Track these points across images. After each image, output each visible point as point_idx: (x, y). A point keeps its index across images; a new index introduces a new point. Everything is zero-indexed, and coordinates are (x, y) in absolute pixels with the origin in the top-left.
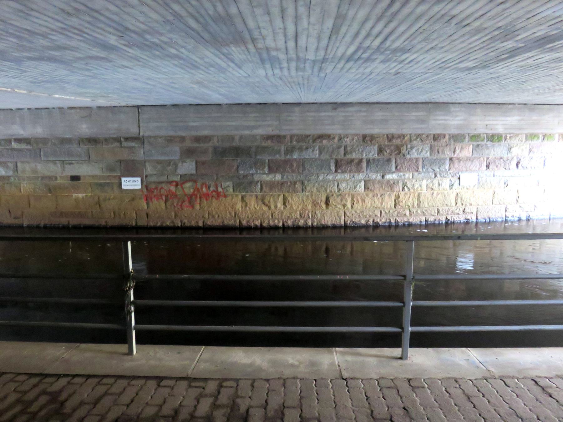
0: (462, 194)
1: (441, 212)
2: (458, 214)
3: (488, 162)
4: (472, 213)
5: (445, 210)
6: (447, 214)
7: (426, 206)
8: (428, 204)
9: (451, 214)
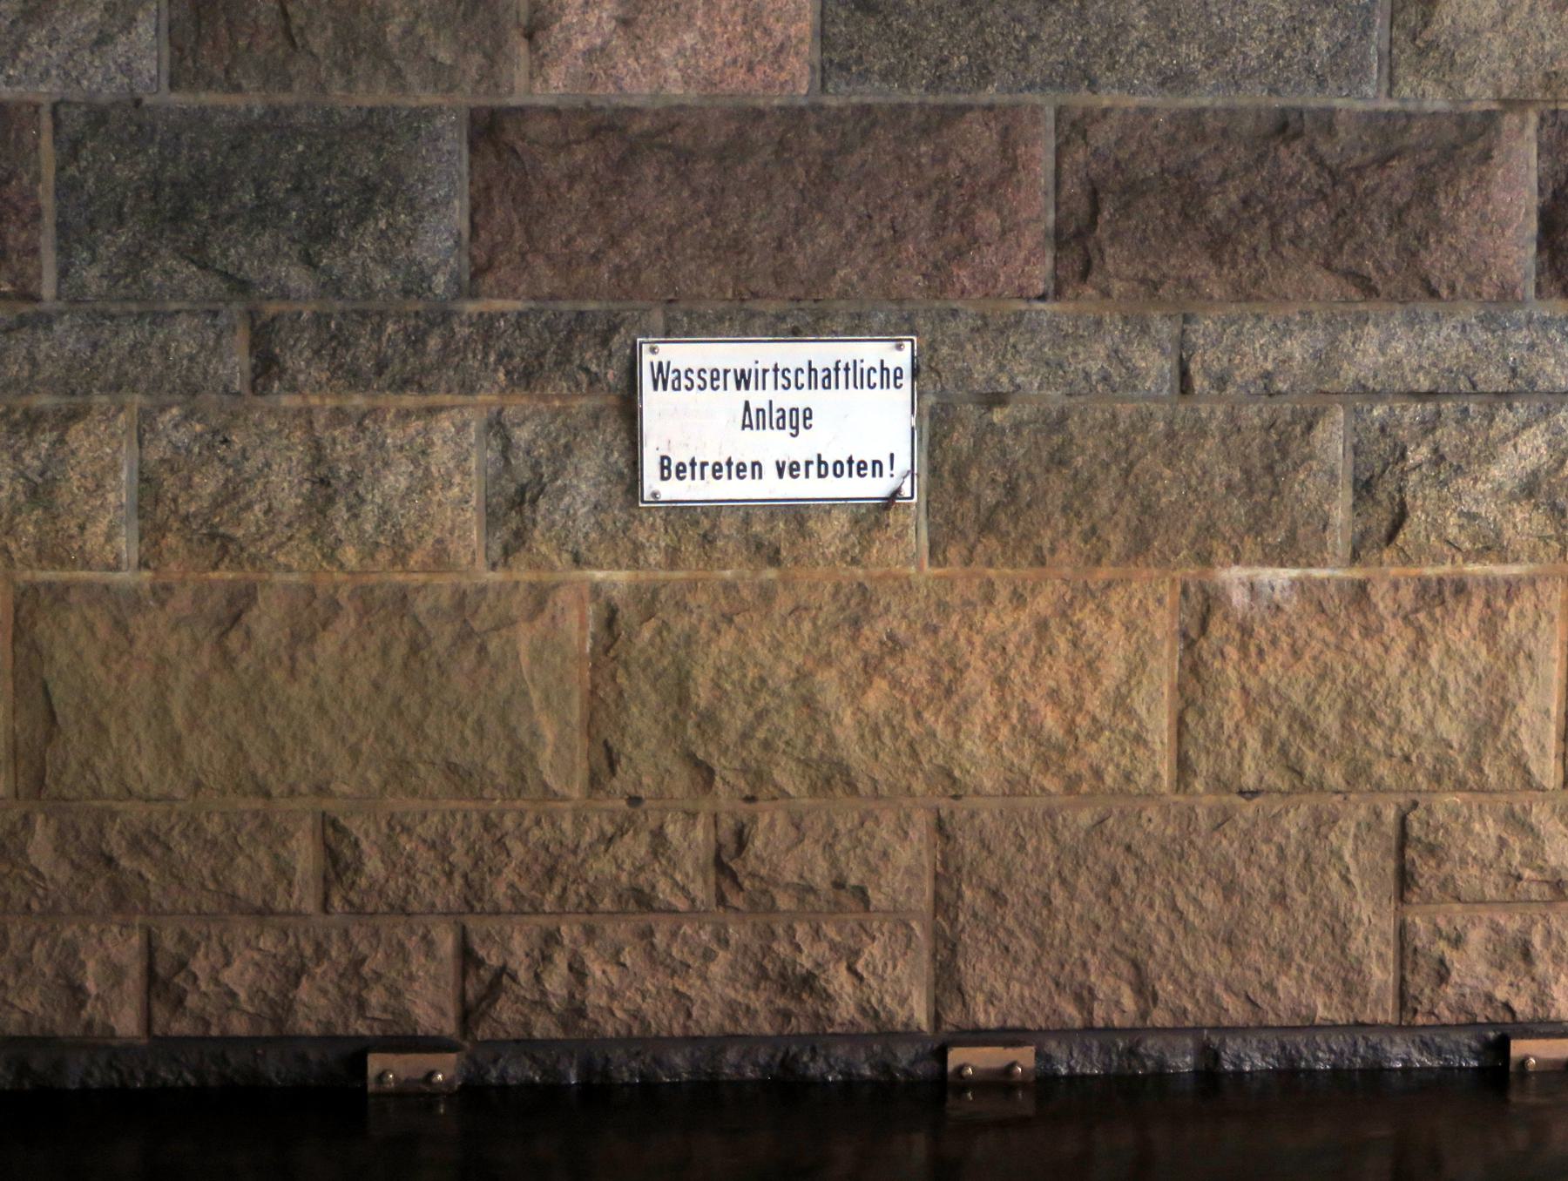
0: (681, 624)
1: (374, 865)
2: (643, 900)
3: (1072, 187)
4: (861, 893)
5: (440, 846)
6: (473, 897)
7: (144, 767)
8: (173, 747)
9: (523, 906)
